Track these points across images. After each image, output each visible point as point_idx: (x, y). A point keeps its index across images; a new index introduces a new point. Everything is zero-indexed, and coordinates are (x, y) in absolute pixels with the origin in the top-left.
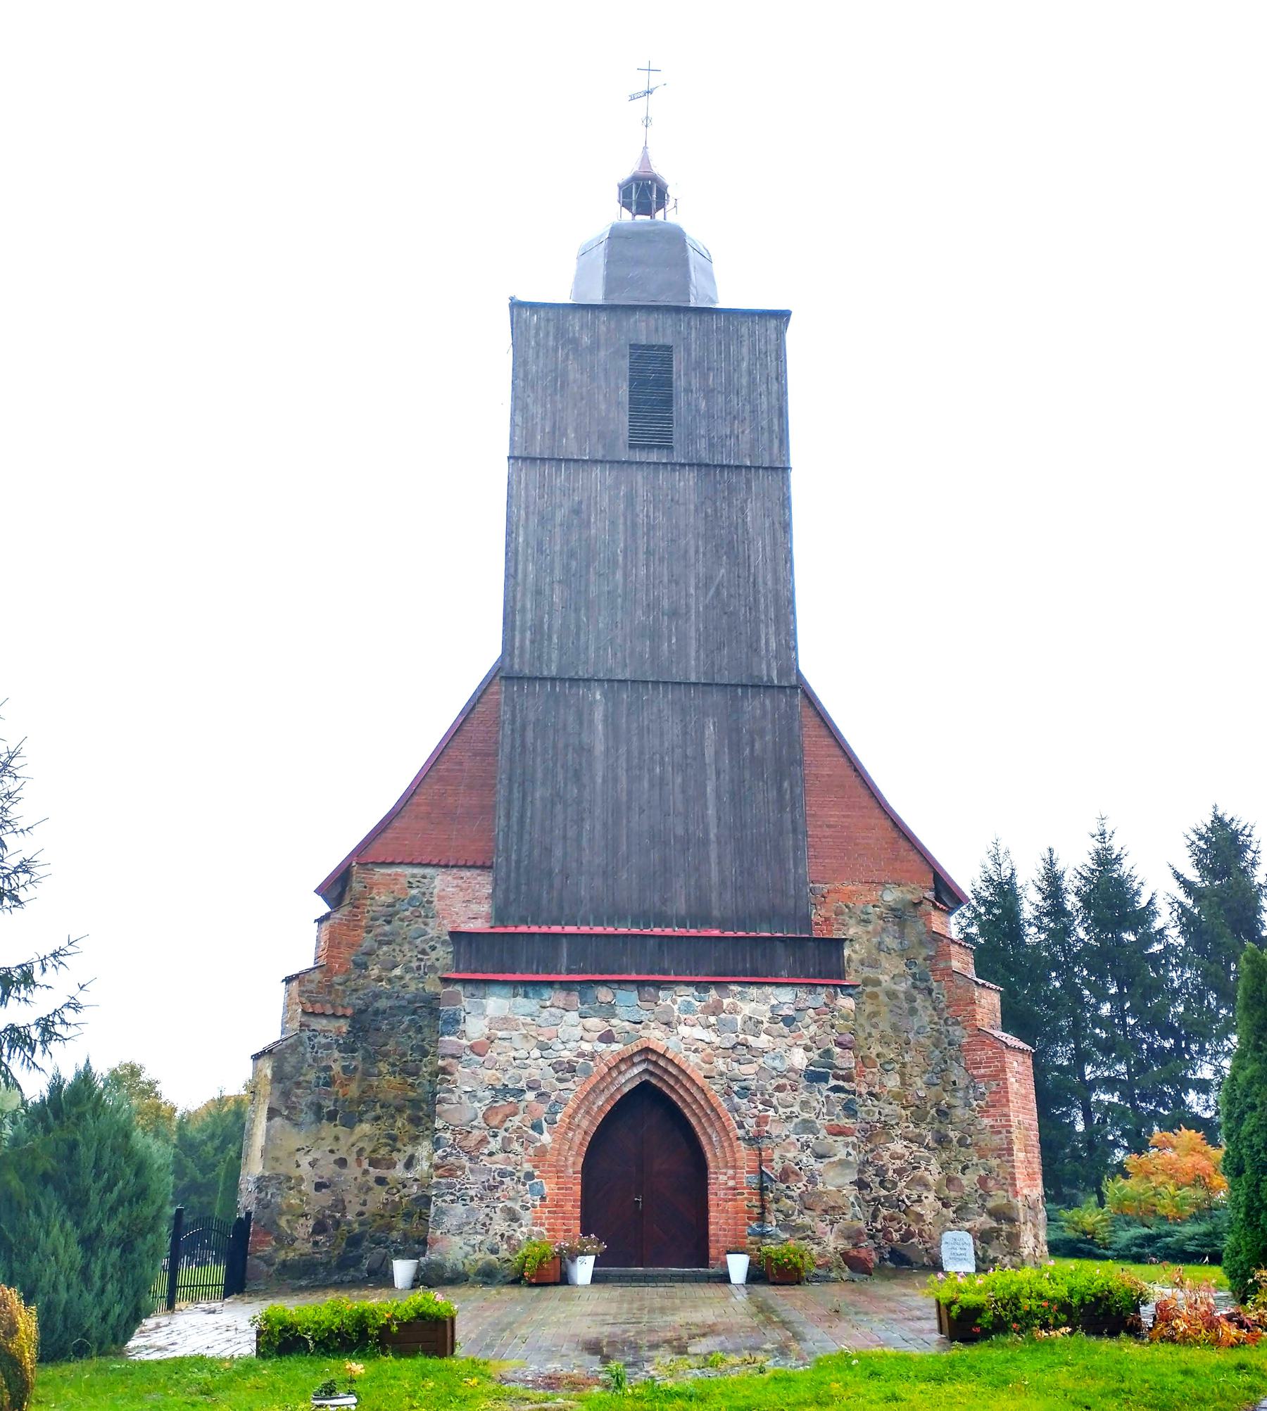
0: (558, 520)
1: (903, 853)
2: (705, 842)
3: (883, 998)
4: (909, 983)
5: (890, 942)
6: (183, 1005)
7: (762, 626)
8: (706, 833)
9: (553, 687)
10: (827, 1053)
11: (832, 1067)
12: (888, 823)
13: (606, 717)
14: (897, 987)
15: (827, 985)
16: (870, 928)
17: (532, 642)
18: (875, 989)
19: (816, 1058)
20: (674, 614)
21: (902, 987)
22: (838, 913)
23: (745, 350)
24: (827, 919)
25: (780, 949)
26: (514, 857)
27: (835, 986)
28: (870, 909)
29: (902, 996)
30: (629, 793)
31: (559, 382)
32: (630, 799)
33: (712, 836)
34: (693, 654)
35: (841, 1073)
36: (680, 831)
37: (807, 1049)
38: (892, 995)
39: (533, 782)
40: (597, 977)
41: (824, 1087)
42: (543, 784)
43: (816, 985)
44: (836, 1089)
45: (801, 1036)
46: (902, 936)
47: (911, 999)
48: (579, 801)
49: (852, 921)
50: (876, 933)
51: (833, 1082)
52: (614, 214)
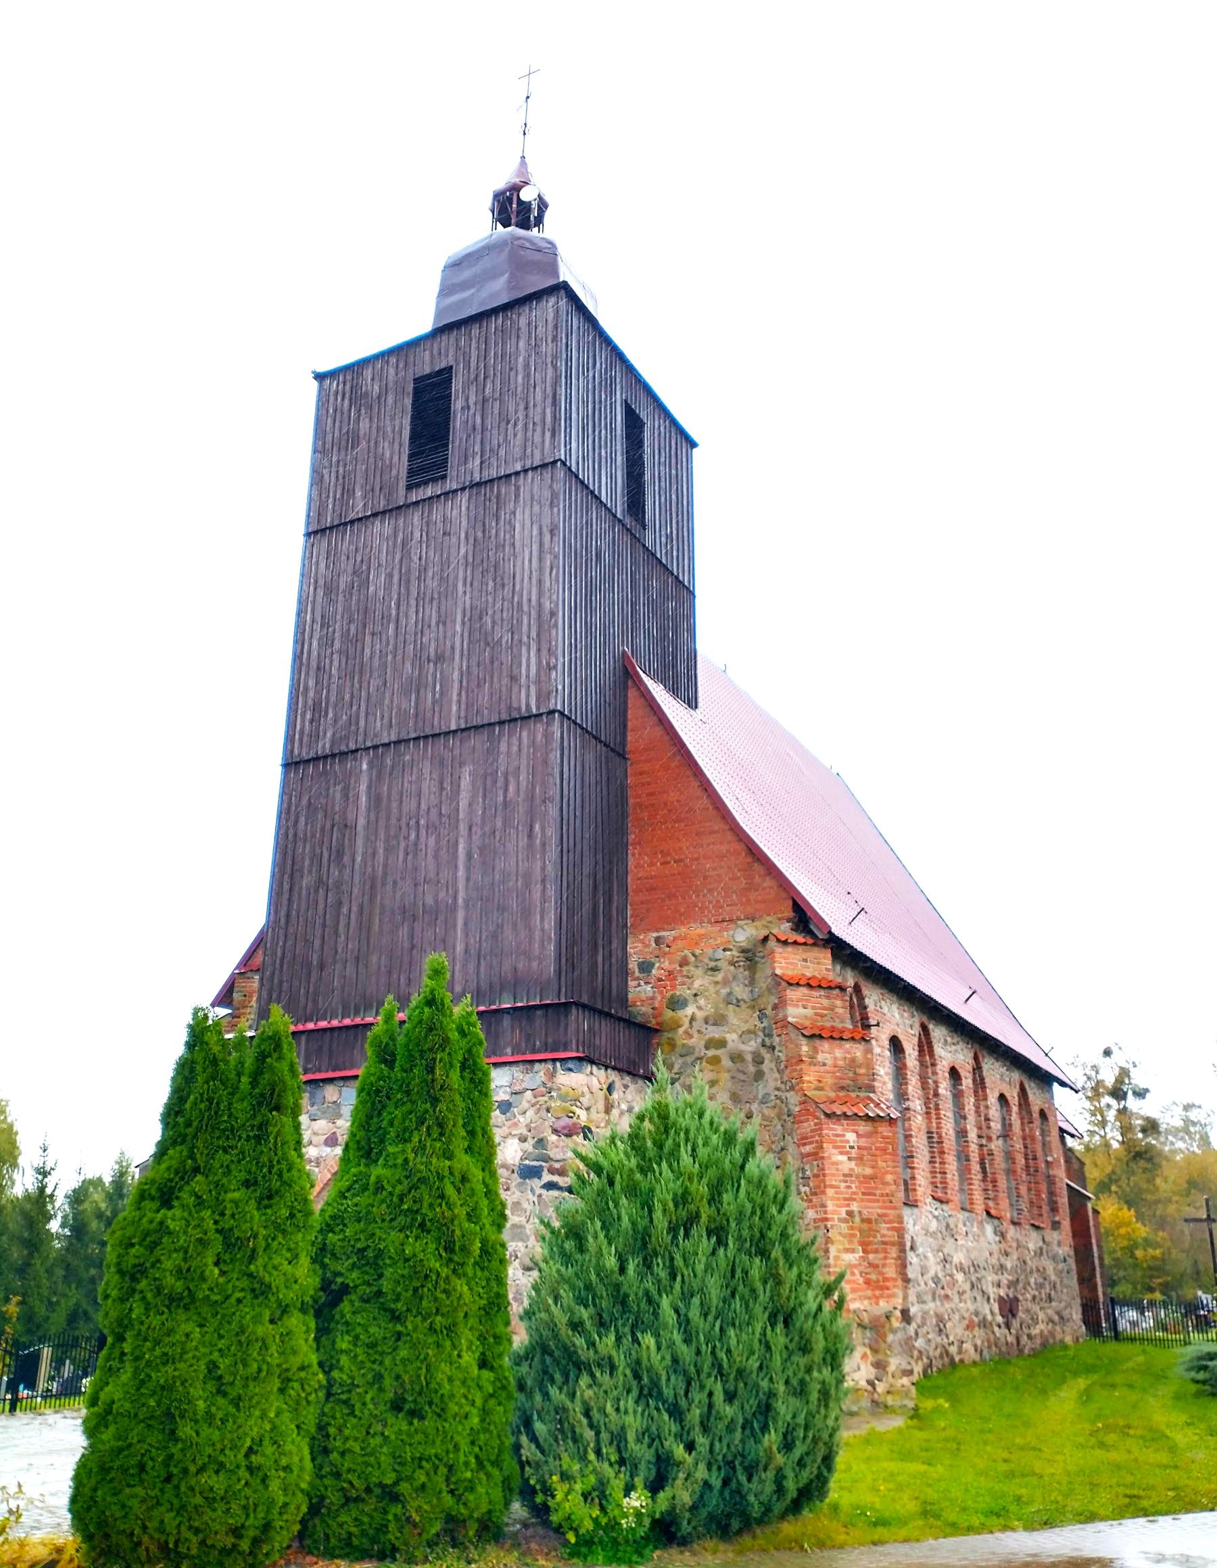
0: (342, 586)
1: (757, 879)
2: (453, 909)
3: (726, 1062)
4: (759, 1040)
5: (741, 991)
6: (97, 1125)
7: (524, 649)
8: (455, 898)
9: (325, 765)
10: (541, 1143)
11: (547, 1159)
12: (739, 847)
13: (369, 787)
14: (743, 1047)
15: (545, 1061)
16: (719, 977)
17: (312, 721)
18: (718, 1052)
19: (531, 1149)
20: (440, 658)
21: (752, 1045)
22: (684, 962)
23: (522, 344)
24: (670, 973)
25: (506, 1021)
26: (279, 954)
27: (554, 1060)
28: (720, 954)
29: (749, 1058)
30: (385, 866)
31: (352, 439)
32: (385, 874)
33: (460, 901)
34: (455, 697)
35: (557, 1165)
36: (430, 901)
37: (523, 1139)
38: (737, 1057)
39: (301, 870)
40: (331, 1075)
41: (536, 1183)
42: (310, 872)
43: (532, 1062)
44: (550, 1186)
45: (516, 1125)
46: (752, 982)
47: (758, 1060)
48: (338, 884)
49: (699, 972)
50: (726, 982)
51: (547, 1177)
52: (479, 227)
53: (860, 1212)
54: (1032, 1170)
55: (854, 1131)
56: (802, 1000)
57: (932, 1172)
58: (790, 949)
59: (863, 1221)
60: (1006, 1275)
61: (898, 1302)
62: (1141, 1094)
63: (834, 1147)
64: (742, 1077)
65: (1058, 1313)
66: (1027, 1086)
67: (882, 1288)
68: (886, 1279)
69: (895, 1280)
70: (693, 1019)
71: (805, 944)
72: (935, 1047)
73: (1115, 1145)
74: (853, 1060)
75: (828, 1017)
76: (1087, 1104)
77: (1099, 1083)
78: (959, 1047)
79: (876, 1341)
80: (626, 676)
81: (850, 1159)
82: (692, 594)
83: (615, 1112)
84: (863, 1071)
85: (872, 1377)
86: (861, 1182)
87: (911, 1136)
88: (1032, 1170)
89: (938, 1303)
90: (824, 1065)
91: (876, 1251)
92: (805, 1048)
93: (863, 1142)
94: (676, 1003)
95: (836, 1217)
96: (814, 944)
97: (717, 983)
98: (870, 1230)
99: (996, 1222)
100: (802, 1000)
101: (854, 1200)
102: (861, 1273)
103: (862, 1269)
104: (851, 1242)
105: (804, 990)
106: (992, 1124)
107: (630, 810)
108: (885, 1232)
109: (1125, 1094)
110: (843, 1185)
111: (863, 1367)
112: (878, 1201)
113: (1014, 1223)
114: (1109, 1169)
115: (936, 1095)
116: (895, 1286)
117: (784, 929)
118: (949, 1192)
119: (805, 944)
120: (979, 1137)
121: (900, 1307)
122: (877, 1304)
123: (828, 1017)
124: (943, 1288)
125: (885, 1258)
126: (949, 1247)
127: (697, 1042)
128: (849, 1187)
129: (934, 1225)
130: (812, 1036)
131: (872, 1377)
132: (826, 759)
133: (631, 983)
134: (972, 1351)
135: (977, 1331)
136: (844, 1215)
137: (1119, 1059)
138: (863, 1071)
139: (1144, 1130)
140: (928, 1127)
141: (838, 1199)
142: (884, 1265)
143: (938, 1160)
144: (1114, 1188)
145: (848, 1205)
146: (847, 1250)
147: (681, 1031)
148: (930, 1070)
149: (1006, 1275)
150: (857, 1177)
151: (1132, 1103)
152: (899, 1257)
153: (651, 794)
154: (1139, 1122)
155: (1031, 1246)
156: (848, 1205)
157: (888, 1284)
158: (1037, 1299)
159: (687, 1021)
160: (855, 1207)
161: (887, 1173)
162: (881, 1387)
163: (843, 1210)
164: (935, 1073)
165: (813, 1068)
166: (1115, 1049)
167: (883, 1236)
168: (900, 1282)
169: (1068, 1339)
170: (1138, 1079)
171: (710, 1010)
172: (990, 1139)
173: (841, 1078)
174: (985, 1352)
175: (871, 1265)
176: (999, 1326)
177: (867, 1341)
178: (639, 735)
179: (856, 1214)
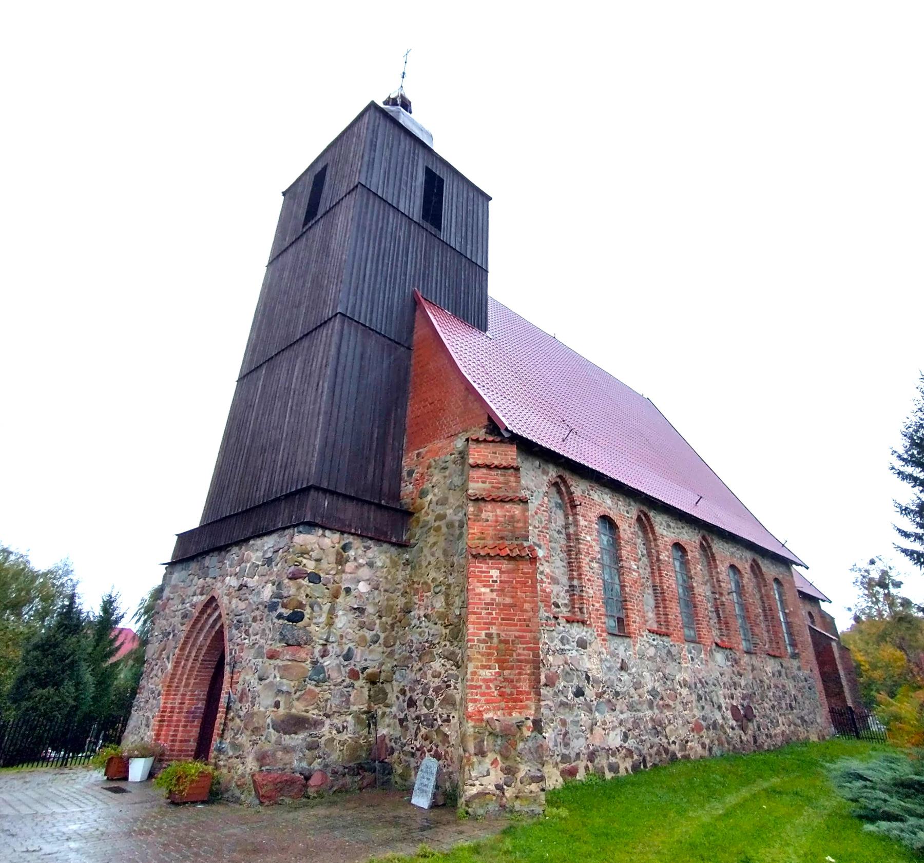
3: (444, 529)
22: (429, 467)
24: (422, 474)
28: (448, 458)
38: (450, 525)
49: (437, 471)
50: (450, 476)
53: (498, 635)
54: (769, 618)
55: (497, 569)
56: (481, 478)
57: (657, 614)
58: (482, 445)
59: (501, 642)
60: (739, 690)
61: (531, 713)
62: (898, 585)
63: (478, 581)
64: (452, 538)
65: (802, 718)
66: (760, 562)
67: (515, 700)
68: (521, 693)
69: (528, 693)
70: (430, 503)
71: (493, 441)
72: (656, 528)
73: (886, 614)
74: (512, 517)
75: (503, 489)
76: (866, 592)
77: (871, 579)
78: (684, 531)
79: (506, 748)
80: (416, 303)
81: (492, 591)
82: (487, 272)
83: (350, 566)
84: (520, 525)
85: (501, 782)
86: (501, 610)
87: (624, 586)
88: (769, 618)
89: (657, 711)
90: (487, 521)
91: (512, 668)
92: (471, 509)
93: (505, 577)
94: (423, 494)
95: (476, 638)
96: (501, 442)
97: (445, 477)
98: (507, 649)
99: (728, 652)
100: (481, 478)
101: (494, 624)
102: (496, 686)
103: (498, 683)
104: (489, 660)
105: (484, 471)
106: (722, 584)
107: (411, 378)
108: (521, 651)
109: (888, 585)
110: (484, 612)
111: (492, 772)
112: (516, 625)
113: (748, 652)
114: (882, 628)
115: (658, 560)
116: (527, 699)
117: (481, 434)
118: (671, 628)
119: (493, 441)
120: (713, 593)
121: (532, 718)
122: (510, 715)
123: (503, 489)
124: (662, 699)
125: (520, 674)
126: (671, 668)
127: (431, 518)
128: (491, 614)
129: (651, 652)
130: (477, 500)
131: (501, 782)
132: (640, 391)
133: (403, 485)
134: (699, 749)
135: (704, 733)
136: (483, 637)
137: (880, 565)
138: (520, 525)
139: (902, 605)
140: (654, 583)
141: (479, 623)
142: (518, 681)
143: (661, 605)
144: (888, 639)
145: (488, 629)
146: (484, 667)
147: (423, 511)
148: (653, 544)
149: (739, 690)
150: (498, 605)
151: (893, 590)
152: (533, 674)
153: (422, 366)
154: (899, 601)
155: (769, 669)
156: (488, 629)
157: (521, 697)
158: (777, 708)
159: (427, 504)
160: (494, 630)
161: (525, 602)
162: (509, 792)
163: (484, 632)
164: (657, 546)
165: (478, 524)
166: (876, 560)
167: (519, 655)
168: (532, 695)
169: (814, 738)
170: (894, 575)
171: (440, 495)
172: (721, 594)
173: (500, 530)
174: (715, 749)
175: (506, 680)
176: (733, 729)
177: (497, 748)
178: (420, 332)
179: (494, 635)
